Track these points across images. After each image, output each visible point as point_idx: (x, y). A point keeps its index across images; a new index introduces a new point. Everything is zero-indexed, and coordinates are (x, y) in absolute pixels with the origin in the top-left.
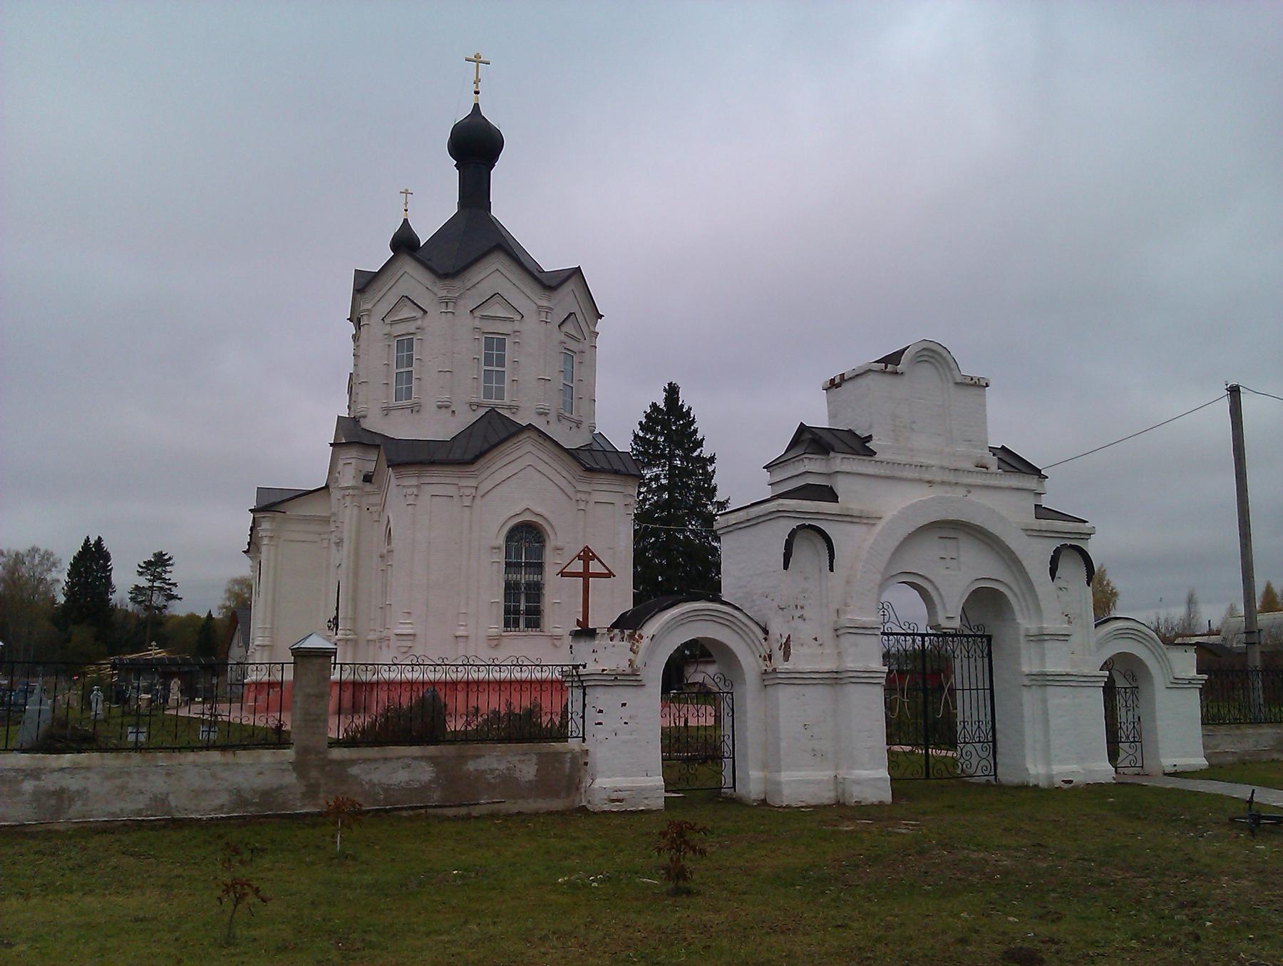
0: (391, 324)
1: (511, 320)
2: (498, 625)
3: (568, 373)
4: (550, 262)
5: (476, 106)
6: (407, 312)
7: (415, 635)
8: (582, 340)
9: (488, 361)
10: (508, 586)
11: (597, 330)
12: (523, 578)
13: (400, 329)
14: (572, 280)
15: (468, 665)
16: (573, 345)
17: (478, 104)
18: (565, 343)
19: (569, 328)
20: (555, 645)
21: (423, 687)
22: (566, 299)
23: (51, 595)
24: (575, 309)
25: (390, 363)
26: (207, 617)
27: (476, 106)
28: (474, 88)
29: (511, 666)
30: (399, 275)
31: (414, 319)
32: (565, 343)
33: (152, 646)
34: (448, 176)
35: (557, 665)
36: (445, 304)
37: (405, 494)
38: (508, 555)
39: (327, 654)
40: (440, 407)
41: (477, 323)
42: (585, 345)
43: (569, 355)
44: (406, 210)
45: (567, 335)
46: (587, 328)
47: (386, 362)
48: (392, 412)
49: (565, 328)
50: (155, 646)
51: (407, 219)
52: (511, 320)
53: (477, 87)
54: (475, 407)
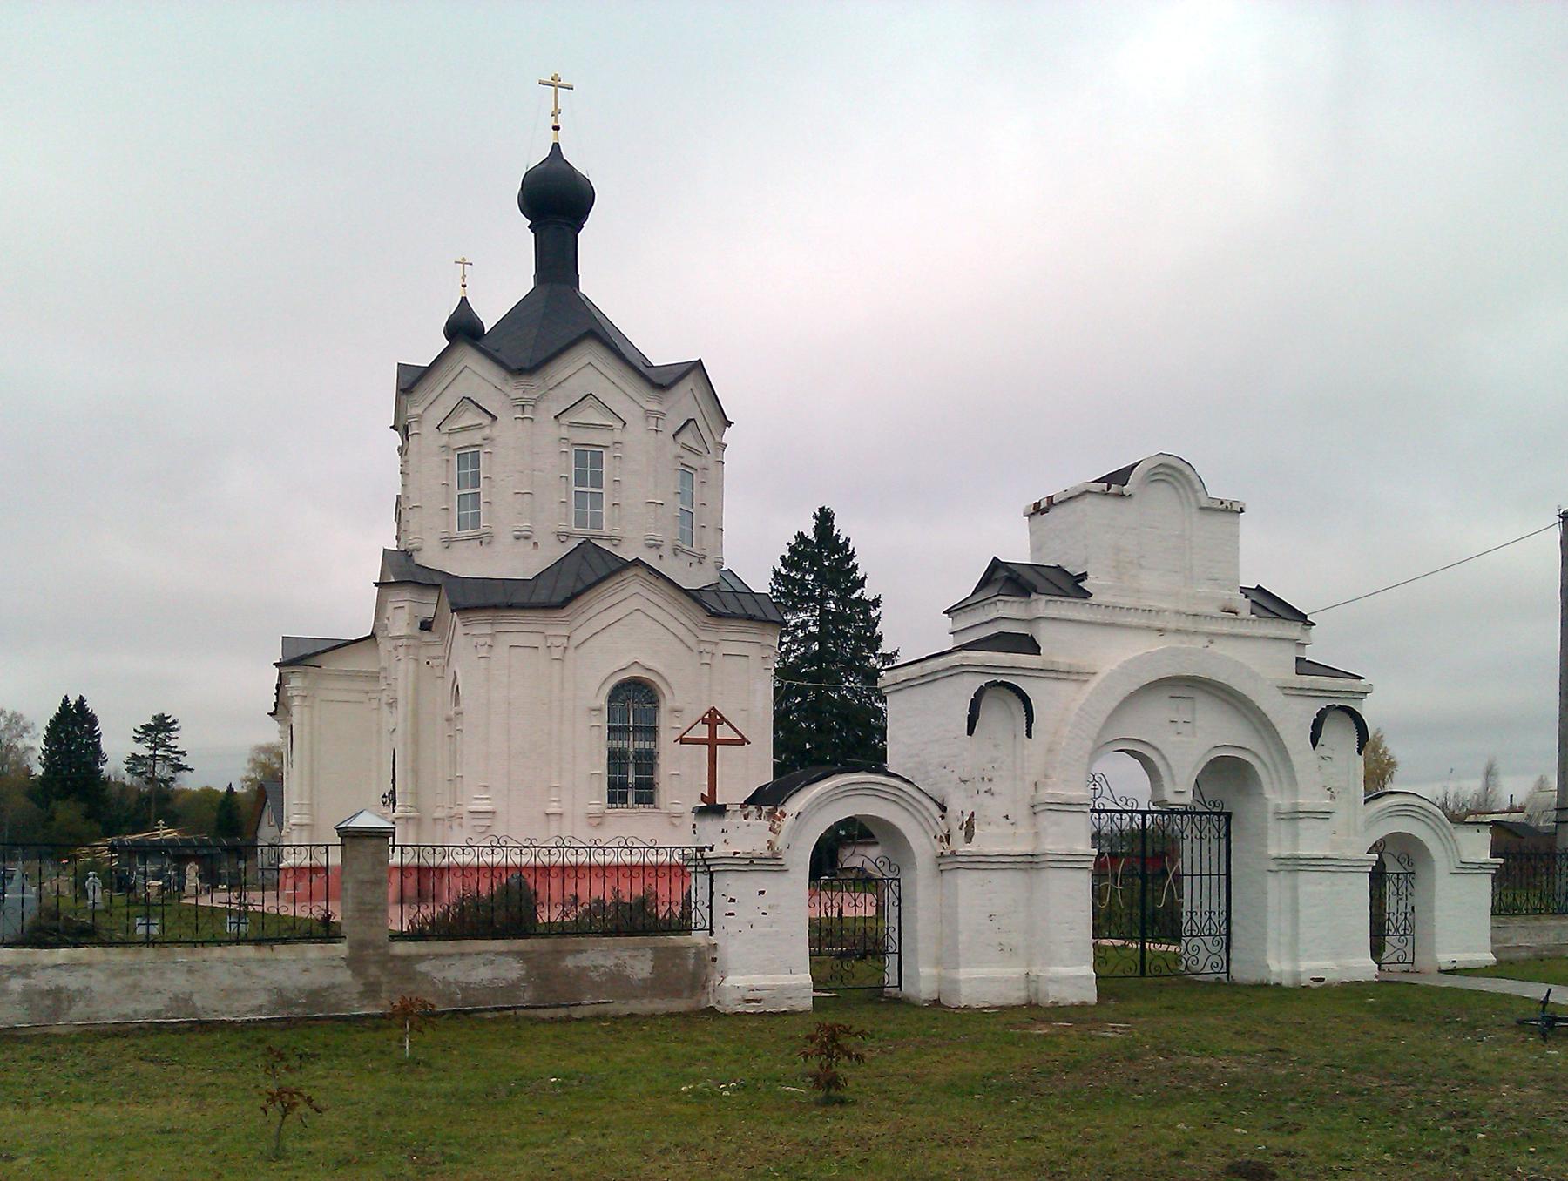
1: (610, 428)
4: (660, 352)
5: (556, 147)
6: (470, 418)
8: (705, 453)
16: (692, 460)
19: (687, 438)
20: (673, 824)
22: (683, 402)
25: (450, 482)
28: (552, 122)
32: (682, 458)
36: (520, 408)
39: (384, 834)
41: (564, 432)
42: (709, 460)
45: (685, 447)
52: (610, 428)
53: (556, 121)
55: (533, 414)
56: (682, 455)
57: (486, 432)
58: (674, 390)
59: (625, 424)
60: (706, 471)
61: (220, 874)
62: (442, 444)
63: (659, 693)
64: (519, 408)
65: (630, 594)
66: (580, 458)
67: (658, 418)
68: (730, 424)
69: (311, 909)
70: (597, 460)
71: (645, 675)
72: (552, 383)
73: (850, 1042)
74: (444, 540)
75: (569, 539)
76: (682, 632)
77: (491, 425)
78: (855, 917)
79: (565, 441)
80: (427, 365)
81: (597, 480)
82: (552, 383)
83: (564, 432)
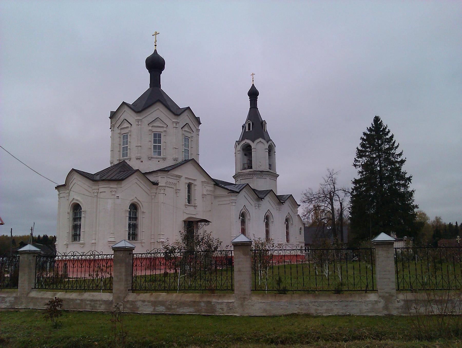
0: (152, 127)
1: (163, 127)
2: (84, 239)
3: (186, 145)
4: (182, 106)
5: (156, 50)
6: (126, 125)
7: (96, 243)
8: (192, 132)
9: (155, 142)
10: (129, 225)
11: (199, 129)
12: (132, 222)
13: (155, 129)
14: (187, 111)
15: (296, 250)
16: (189, 135)
17: (156, 50)
18: (184, 134)
19: (186, 129)
20: (142, 246)
21: (98, 261)
22: (185, 118)
23: (349, 221)
24: (188, 121)
25: (121, 143)
26: (43, 236)
27: (156, 50)
28: (155, 44)
29: (146, 253)
30: (122, 112)
31: (128, 127)
32: (184, 134)
33: (457, 238)
34: (147, 75)
35: (140, 254)
36: (137, 122)
37: (93, 192)
38: (130, 214)
39: (131, 250)
40: (137, 159)
41: (150, 128)
42: (194, 134)
43: (187, 139)
44: (253, 81)
45: (185, 131)
46: (195, 128)
47: (119, 143)
48: (153, 159)
49: (183, 129)
50: (459, 238)
51: (253, 84)
52: (163, 127)
53: (156, 44)
54: (150, 159)
55: (141, 123)
56: (184, 133)
57: (129, 129)
58: (181, 116)
59: (167, 126)
60: (193, 138)
61: (4, 277)
62: (129, 130)
63: (137, 207)
64: (137, 122)
65: (134, 179)
66: (155, 135)
67: (176, 124)
68: (201, 124)
69: (290, 253)
70: (160, 136)
71: (138, 202)
72: (117, 119)
73: (422, 283)
74: (149, 158)
75: (151, 159)
76: (146, 190)
77: (131, 127)
78: (160, 274)
79: (151, 131)
80: (115, 111)
81: (160, 142)
82: (117, 119)
83: (150, 128)
